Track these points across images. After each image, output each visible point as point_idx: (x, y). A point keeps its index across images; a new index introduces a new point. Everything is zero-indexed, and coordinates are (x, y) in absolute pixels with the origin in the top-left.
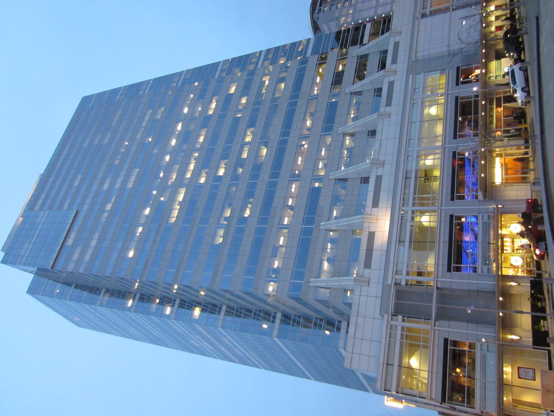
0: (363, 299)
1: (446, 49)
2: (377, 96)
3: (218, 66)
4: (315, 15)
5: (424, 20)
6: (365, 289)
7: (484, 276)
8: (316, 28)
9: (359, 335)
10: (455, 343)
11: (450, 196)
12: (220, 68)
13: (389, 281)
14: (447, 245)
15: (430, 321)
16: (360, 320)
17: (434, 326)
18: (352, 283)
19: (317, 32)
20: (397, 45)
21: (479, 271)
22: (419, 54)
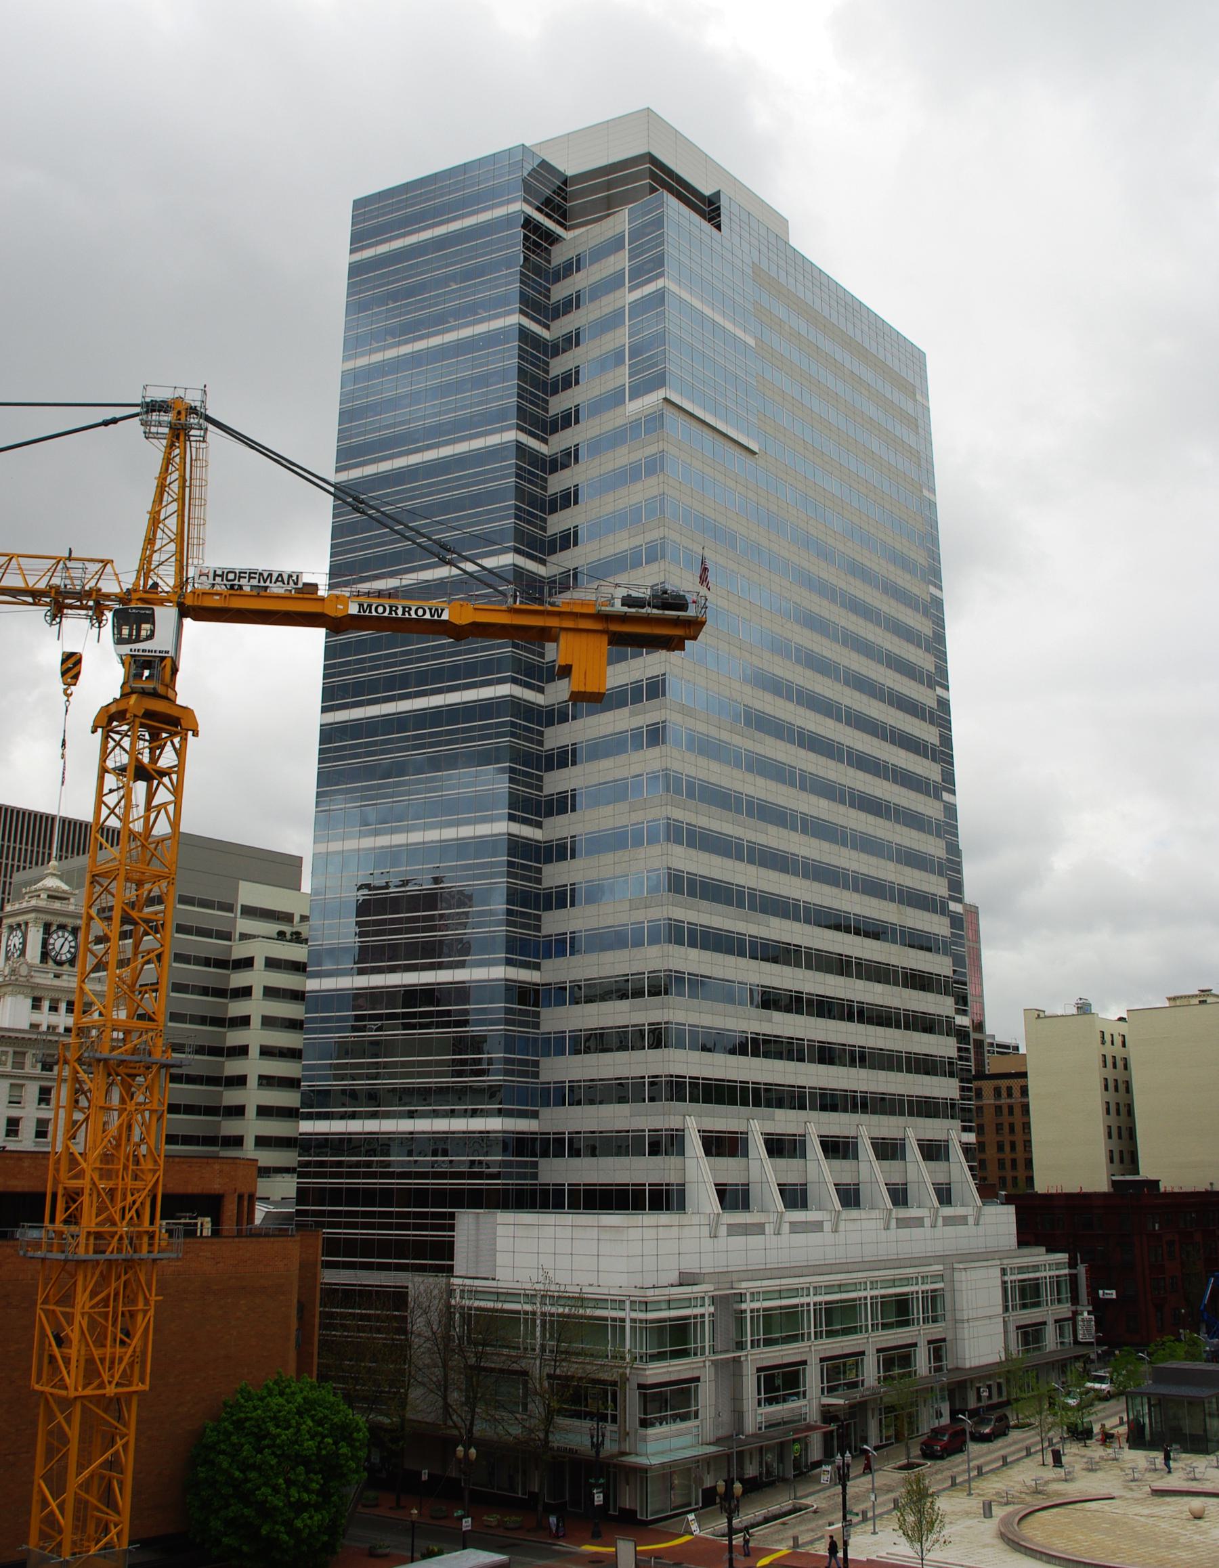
13: (744, 1285)
20: (817, 1227)
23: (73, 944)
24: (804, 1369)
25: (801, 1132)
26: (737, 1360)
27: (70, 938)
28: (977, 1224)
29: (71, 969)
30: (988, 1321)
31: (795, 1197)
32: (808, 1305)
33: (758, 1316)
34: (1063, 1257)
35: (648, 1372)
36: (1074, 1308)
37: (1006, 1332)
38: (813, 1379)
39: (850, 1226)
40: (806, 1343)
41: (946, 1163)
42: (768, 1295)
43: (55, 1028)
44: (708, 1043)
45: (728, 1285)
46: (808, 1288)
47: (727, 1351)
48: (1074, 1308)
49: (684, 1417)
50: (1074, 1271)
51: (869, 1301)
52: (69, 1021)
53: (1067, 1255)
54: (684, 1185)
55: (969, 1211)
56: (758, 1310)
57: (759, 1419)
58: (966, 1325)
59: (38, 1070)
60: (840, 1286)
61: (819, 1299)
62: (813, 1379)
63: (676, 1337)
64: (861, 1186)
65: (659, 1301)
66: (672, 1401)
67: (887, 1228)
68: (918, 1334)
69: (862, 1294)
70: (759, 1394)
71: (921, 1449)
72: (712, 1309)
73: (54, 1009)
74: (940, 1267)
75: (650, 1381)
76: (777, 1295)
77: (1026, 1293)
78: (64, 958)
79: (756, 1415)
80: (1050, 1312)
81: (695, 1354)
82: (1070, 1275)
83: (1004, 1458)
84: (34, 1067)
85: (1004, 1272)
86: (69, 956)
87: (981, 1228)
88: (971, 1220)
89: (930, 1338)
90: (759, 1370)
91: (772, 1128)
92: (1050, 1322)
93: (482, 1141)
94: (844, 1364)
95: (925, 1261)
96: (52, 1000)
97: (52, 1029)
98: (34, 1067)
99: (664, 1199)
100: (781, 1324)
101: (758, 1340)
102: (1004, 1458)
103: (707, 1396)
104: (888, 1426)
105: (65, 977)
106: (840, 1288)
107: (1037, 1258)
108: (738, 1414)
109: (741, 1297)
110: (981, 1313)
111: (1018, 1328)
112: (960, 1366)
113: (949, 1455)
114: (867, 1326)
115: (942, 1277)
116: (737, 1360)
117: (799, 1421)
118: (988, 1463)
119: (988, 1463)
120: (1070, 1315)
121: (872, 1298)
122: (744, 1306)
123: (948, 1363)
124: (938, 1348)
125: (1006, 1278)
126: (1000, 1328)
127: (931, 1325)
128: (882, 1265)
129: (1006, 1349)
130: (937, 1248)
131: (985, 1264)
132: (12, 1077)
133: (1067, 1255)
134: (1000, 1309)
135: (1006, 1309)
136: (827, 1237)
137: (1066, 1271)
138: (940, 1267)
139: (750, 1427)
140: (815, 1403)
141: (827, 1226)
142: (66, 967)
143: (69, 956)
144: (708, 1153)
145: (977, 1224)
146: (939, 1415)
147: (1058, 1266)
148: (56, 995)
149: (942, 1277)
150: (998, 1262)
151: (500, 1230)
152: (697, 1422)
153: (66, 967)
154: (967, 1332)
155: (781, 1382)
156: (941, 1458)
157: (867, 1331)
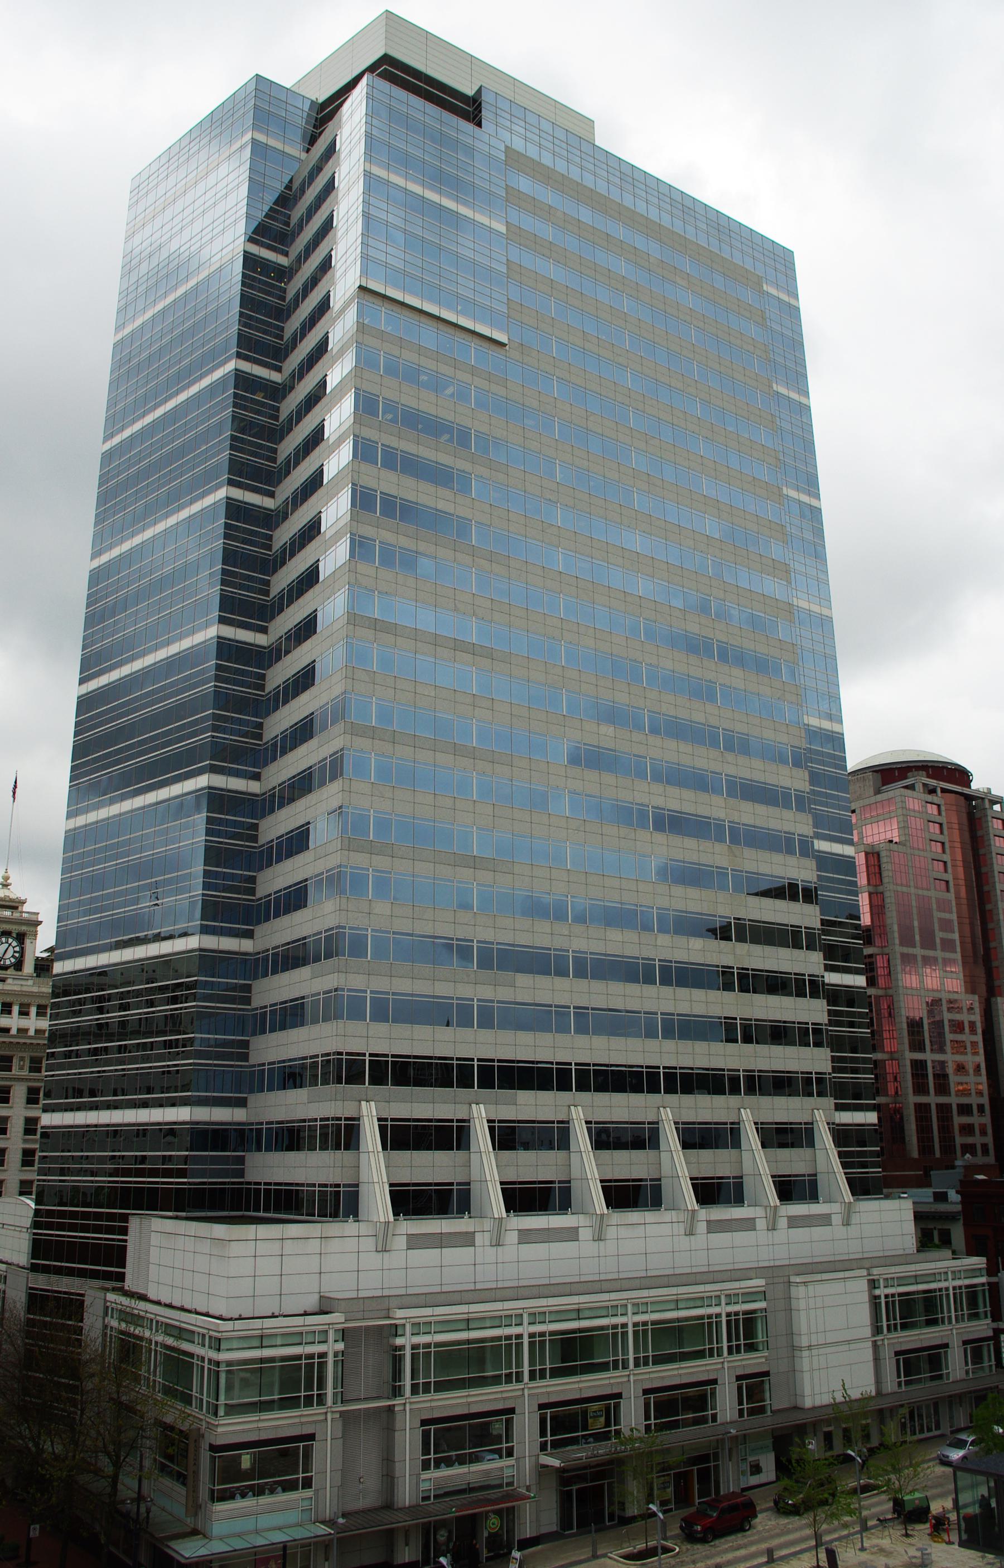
0: (351, 1244)
1: (805, 1342)
2: (752, 1412)
3: (809, 494)
4: (922, 779)
5: (863, 1285)
6: (369, 1244)
7: (418, 1484)
8: (890, 774)
9: (289, 1247)
10: (308, 1453)
11: (544, 1400)
12: (804, 498)
13: (400, 1313)
14: (465, 1411)
15: (339, 1404)
16: (314, 1245)
17: (333, 1412)
18: (382, 1220)
19: (879, 776)
20: (825, 1220)
21: (426, 1475)
22: (802, 1288)
23: (17, 949)
24: (946, 1353)
25: (806, 1118)
26: (390, 1409)
27: (15, 944)
28: (847, 1223)
29: (15, 973)
30: (846, 1347)
31: (710, 1192)
32: (947, 1289)
33: (645, 1331)
34: (979, 1262)
35: (220, 1430)
36: (995, 1325)
37: (877, 1359)
38: (526, 1430)
39: (623, 1232)
40: (716, 1359)
41: (734, 1152)
42: (902, 1281)
43: (26, 1030)
44: (384, 1010)
45: (383, 1313)
46: (719, 1297)
47: (378, 1398)
48: (995, 1325)
49: (290, 1486)
50: (994, 1279)
51: (951, 1292)
52: (44, 1024)
53: (984, 1260)
54: (815, 1175)
55: (834, 1208)
56: (893, 1295)
57: (424, 1486)
58: (806, 1353)
59: (25, 1073)
60: (916, 1276)
61: (958, 1283)
62: (526, 1430)
63: (295, 1381)
64: (663, 1182)
65: (484, 1318)
66: (282, 1463)
67: (690, 1233)
68: (724, 1368)
69: (943, 1285)
70: (899, 1376)
71: (681, 1527)
72: (340, 1346)
73: (24, 1013)
74: (761, 1282)
75: (220, 1441)
76: (463, 1326)
77: (905, 1309)
78: (8, 962)
79: (416, 1480)
80: (953, 1333)
81: (943, 1323)
82: (989, 1284)
83: (770, 1552)
84: (21, 1068)
85: (873, 1284)
86: (13, 960)
87: (853, 1231)
88: (836, 1219)
89: (740, 1372)
90: (897, 1353)
91: (689, 1116)
92: (956, 1343)
93: (169, 1132)
94: (585, 1412)
95: (745, 1274)
96: (21, 1005)
97: (22, 1031)
98: (21, 1068)
99: (339, 1203)
100: (470, 1362)
101: (646, 1358)
102: (770, 1552)
103: (326, 1458)
104: (664, 1487)
105: (9, 981)
106: (578, 1313)
107: (939, 1264)
108: (389, 1479)
109: (395, 1330)
110: (831, 1338)
111: (897, 1353)
112: (799, 1404)
113: (716, 1537)
114: (950, 1318)
115: (764, 1295)
116: (390, 1409)
117: (500, 1486)
118: (781, 1547)
119: (781, 1547)
120: (990, 1333)
121: (954, 1288)
122: (399, 1341)
123: (776, 1399)
124: (753, 1387)
125: (877, 1292)
126: (868, 1354)
127: (743, 1355)
128: (457, 1297)
129: (878, 1381)
130: (765, 1257)
131: (841, 1275)
132: (11, 1079)
133: (984, 1260)
134: (868, 1332)
135: (877, 1330)
136: (837, 1229)
137: (983, 1280)
138: (761, 1282)
139: (406, 1495)
140: (527, 1464)
141: (761, 1224)
142: (11, 971)
143: (13, 960)
144: (686, 1145)
145: (847, 1223)
146: (756, 1469)
147: (973, 1272)
148: (26, 1000)
149: (764, 1295)
150: (864, 1272)
151: (155, 1239)
152: (308, 1493)
153: (11, 971)
154: (806, 1362)
155: (456, 1438)
156: (704, 1540)
157: (950, 1322)
